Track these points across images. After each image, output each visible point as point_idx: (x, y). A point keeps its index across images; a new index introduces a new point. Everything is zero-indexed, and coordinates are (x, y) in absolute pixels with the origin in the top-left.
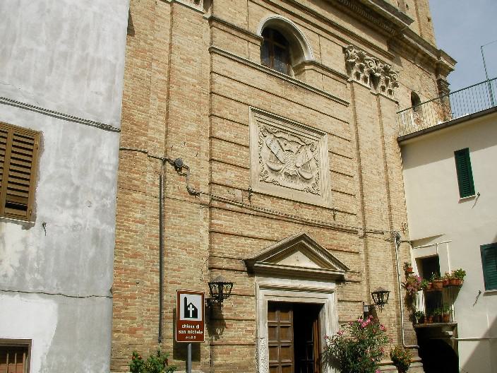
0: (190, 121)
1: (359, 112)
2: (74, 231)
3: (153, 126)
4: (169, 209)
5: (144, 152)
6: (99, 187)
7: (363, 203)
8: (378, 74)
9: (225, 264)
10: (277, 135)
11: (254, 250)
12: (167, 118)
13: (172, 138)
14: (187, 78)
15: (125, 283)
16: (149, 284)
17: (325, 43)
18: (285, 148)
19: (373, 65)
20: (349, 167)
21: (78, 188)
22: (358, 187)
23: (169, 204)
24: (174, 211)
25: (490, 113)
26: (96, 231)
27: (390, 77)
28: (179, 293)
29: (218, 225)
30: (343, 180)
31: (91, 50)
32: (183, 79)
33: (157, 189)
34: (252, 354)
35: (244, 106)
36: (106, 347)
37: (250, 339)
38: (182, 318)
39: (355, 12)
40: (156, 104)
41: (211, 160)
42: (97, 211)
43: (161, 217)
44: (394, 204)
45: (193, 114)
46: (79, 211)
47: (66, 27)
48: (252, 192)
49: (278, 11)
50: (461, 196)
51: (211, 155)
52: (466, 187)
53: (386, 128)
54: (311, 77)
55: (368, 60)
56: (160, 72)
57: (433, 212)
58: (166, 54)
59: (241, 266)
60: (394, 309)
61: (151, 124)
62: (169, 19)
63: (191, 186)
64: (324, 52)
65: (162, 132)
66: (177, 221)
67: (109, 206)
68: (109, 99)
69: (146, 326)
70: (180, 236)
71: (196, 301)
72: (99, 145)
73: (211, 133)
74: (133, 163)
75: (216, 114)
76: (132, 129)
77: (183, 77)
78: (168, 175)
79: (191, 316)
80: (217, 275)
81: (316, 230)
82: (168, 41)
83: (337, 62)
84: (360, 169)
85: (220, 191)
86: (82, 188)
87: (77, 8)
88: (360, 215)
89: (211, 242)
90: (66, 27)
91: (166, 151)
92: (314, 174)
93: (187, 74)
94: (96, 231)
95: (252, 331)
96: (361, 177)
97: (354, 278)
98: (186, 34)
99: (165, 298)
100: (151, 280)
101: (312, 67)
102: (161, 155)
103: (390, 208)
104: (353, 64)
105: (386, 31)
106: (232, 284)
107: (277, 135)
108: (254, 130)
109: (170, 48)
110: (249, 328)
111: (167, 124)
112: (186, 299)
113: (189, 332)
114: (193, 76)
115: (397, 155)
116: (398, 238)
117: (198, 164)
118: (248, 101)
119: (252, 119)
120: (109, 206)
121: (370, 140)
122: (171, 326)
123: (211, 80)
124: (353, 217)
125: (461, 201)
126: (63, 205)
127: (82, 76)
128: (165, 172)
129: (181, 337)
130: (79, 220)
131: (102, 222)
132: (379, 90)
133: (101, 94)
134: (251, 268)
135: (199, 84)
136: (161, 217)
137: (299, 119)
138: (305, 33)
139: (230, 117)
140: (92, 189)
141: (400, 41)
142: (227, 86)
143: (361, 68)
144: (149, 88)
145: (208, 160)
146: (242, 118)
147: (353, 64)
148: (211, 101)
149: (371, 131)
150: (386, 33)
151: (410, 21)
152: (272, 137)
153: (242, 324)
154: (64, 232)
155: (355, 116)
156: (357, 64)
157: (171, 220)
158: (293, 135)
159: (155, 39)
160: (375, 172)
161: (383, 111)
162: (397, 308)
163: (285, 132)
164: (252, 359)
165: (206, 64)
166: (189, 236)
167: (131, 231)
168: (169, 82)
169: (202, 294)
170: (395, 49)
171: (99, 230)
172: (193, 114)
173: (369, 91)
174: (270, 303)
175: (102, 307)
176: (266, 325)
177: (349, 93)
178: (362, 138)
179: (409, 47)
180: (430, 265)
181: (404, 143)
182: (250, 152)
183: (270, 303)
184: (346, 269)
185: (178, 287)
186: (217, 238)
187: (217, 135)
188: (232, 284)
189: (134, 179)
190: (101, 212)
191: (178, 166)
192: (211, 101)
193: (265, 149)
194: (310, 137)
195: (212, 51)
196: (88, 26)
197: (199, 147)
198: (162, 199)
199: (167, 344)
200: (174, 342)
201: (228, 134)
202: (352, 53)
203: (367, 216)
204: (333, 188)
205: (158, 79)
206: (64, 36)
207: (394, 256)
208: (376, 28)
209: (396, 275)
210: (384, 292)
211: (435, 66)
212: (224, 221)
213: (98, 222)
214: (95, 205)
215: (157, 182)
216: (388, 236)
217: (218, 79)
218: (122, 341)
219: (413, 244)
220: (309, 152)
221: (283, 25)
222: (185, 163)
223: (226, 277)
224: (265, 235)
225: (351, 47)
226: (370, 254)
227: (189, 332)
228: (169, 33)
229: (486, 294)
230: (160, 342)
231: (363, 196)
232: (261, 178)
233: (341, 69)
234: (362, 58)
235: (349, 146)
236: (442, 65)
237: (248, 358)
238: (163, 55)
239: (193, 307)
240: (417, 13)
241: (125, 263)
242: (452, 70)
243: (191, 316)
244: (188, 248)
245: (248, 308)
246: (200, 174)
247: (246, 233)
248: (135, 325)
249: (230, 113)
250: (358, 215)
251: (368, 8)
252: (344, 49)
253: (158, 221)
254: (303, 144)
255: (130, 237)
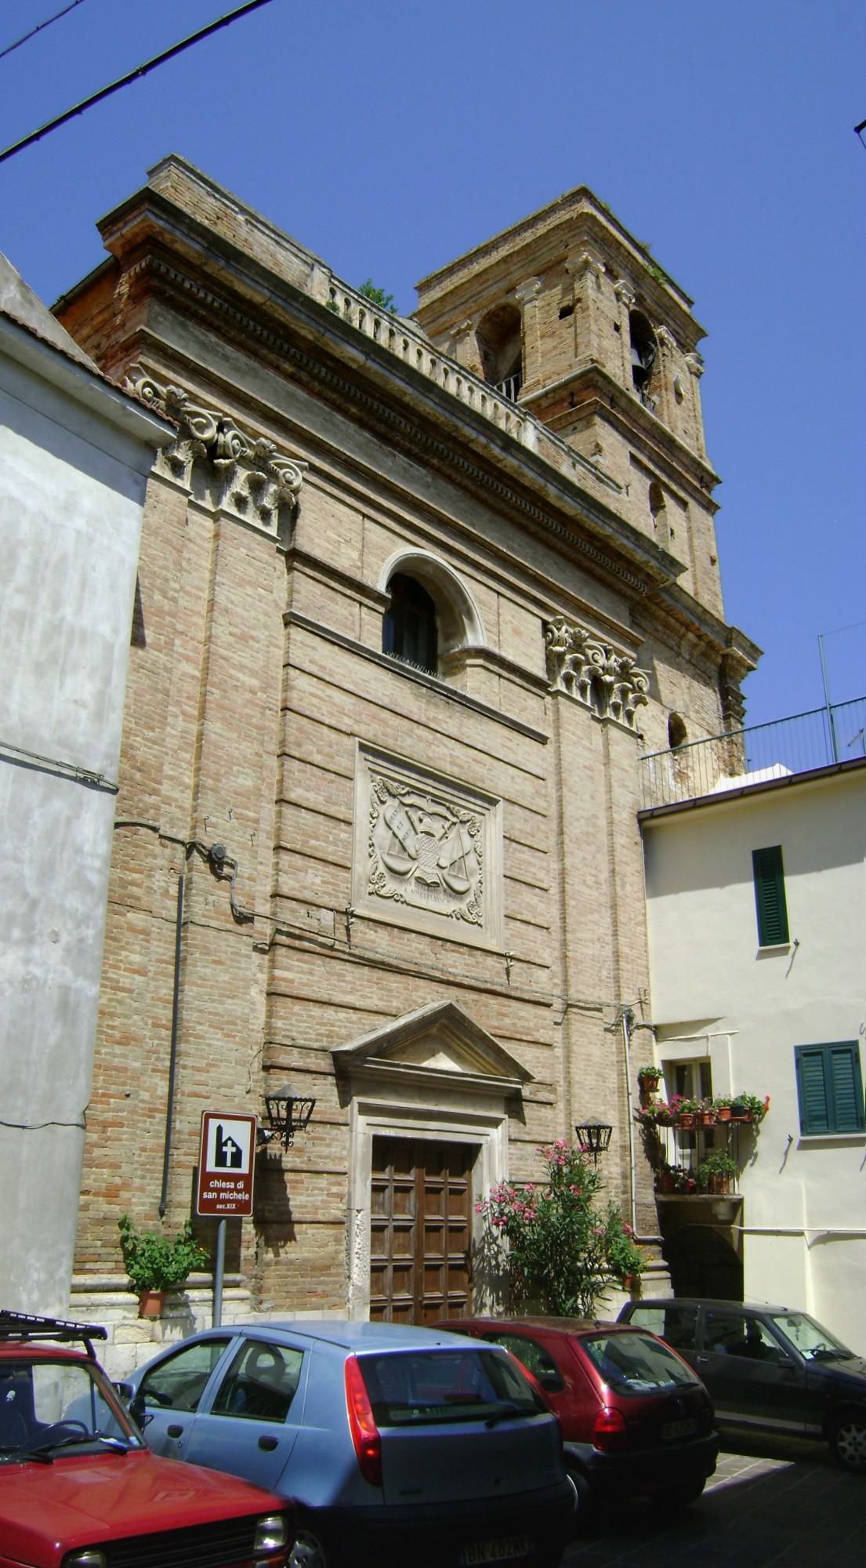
0: (243, 767)
1: (567, 758)
2: (24, 990)
3: (171, 773)
4: (195, 946)
5: (155, 829)
6: (73, 902)
7: (564, 944)
8: (608, 678)
9: (295, 1059)
10: (408, 800)
11: (355, 1036)
12: (198, 757)
13: (208, 800)
14: (240, 676)
15: (103, 1095)
16: (146, 1096)
17: (509, 611)
18: (420, 827)
19: (602, 660)
20: (541, 870)
21: (34, 904)
22: (555, 911)
23: (193, 934)
24: (206, 951)
25: (830, 775)
26: (65, 990)
27: (584, 654)
28: (208, 1116)
29: (285, 980)
30: (529, 897)
31: (68, 611)
32: (231, 677)
33: (172, 904)
34: (338, 1241)
35: (345, 738)
36: (69, 1226)
37: (335, 1211)
38: (211, 1167)
39: (455, 467)
40: (179, 726)
41: (278, 848)
42: (68, 951)
43: (179, 961)
44: (625, 950)
45: (248, 749)
46: (36, 952)
47: (25, 558)
48: (353, 915)
49: (423, 542)
50: (762, 943)
51: (278, 837)
52: (773, 927)
53: (617, 791)
54: (474, 682)
55: (591, 648)
56: (188, 659)
57: (744, 987)
58: (201, 622)
59: (325, 1064)
60: (618, 1160)
61: (168, 770)
62: (210, 546)
63: (239, 900)
64: (506, 630)
65: (187, 787)
66: (208, 971)
67: (90, 941)
68: (99, 716)
69: (137, 1182)
70: (213, 1001)
71: (240, 1134)
72: (78, 817)
73: (281, 792)
74: (131, 850)
75: (293, 753)
76: (131, 779)
77: (232, 671)
78: (196, 877)
79: (229, 1163)
80: (281, 1082)
81: (472, 996)
82: (206, 595)
83: (532, 651)
84: (563, 873)
85: (293, 911)
86: (42, 904)
87: (46, 520)
88: (557, 968)
89: (270, 1014)
90: (25, 558)
91: (194, 828)
92: (474, 881)
93: (242, 667)
94: (65, 990)
95: (340, 1196)
96: (563, 891)
97: (543, 1096)
98: (242, 582)
99: (177, 1125)
100: (152, 1090)
101: (480, 661)
102: (184, 835)
103: (617, 955)
104: (560, 656)
105: (630, 586)
106: (313, 1101)
107: (408, 800)
108: (363, 788)
109: (211, 609)
110: (334, 1189)
111: (198, 770)
112: (220, 1130)
113: (223, 1195)
114: (254, 674)
115: (635, 848)
116: (630, 1019)
117: (254, 855)
118: (356, 729)
119: (360, 764)
120: (90, 941)
121: (585, 814)
122: (188, 1181)
123: (286, 680)
124: (542, 974)
125: (761, 955)
126: (6, 938)
127: (51, 665)
128: (190, 870)
129: (208, 1205)
130: (37, 971)
131: (77, 974)
132: (227, 505)
133: (84, 706)
134: (351, 1072)
135: (264, 690)
136: (179, 961)
137: (449, 769)
138: (473, 589)
139: (317, 759)
140: (62, 906)
141: (654, 608)
142: (316, 696)
143: (576, 665)
144: (167, 693)
145: (272, 846)
146: (341, 764)
147: (560, 656)
148: (284, 725)
149: (587, 797)
150: (629, 592)
151: (676, 567)
152: (396, 802)
153: (323, 1181)
154: (7, 994)
155: (559, 766)
156: (568, 657)
157: (198, 968)
158: (437, 800)
159: (182, 589)
160: (590, 880)
161: (612, 755)
162: (623, 1160)
163: (422, 793)
164: (337, 1252)
165: (277, 646)
166: (230, 1001)
167: (123, 990)
168: (204, 682)
169: (252, 1120)
170: (644, 624)
171: (69, 988)
172: (248, 749)
173: (185, 500)
174: (377, 1140)
175: (66, 1144)
176: (369, 1183)
177: (551, 716)
178: (569, 811)
179: (672, 621)
180: (687, 1075)
181: (650, 824)
182: (352, 834)
183: (377, 1140)
184: (526, 1077)
185: (210, 1106)
186: (283, 1006)
187: (292, 796)
188: (313, 1101)
189: (133, 883)
190: (76, 952)
191: (216, 861)
192: (284, 725)
193: (381, 829)
194: (467, 807)
195: (291, 620)
196: (63, 559)
197: (257, 821)
198: (181, 925)
199: (176, 1219)
200: (193, 1215)
201: (311, 796)
202: (563, 632)
203: (571, 971)
204: (508, 912)
205: (185, 674)
206: (21, 578)
207: (621, 1051)
208: (610, 579)
209: (623, 1091)
210: (604, 1127)
211: (719, 660)
212: (296, 971)
213: (69, 974)
214: (65, 938)
215: (174, 890)
216: (610, 1016)
217: (302, 682)
218: (91, 1214)
219: (659, 1032)
220: (466, 838)
221: (430, 570)
222: (229, 853)
223: (300, 1087)
224: (374, 1003)
225: (560, 622)
226: (575, 1048)
227: (223, 1195)
228: (207, 575)
229: (804, 1145)
230: (162, 1213)
231: (564, 930)
232: (371, 888)
233: (536, 666)
234: (578, 645)
235: (543, 827)
236: (733, 657)
237: (331, 1248)
238: (196, 624)
239: (234, 1145)
240: (691, 547)
241: (107, 1053)
242: (751, 669)
243: (229, 1163)
244: (226, 1025)
245: (334, 1150)
246: (255, 875)
247: (338, 998)
248: (118, 1180)
249: (319, 752)
250: (553, 968)
251: (599, 540)
252: (545, 623)
253: (172, 968)
254: (455, 820)
255: (118, 1001)
